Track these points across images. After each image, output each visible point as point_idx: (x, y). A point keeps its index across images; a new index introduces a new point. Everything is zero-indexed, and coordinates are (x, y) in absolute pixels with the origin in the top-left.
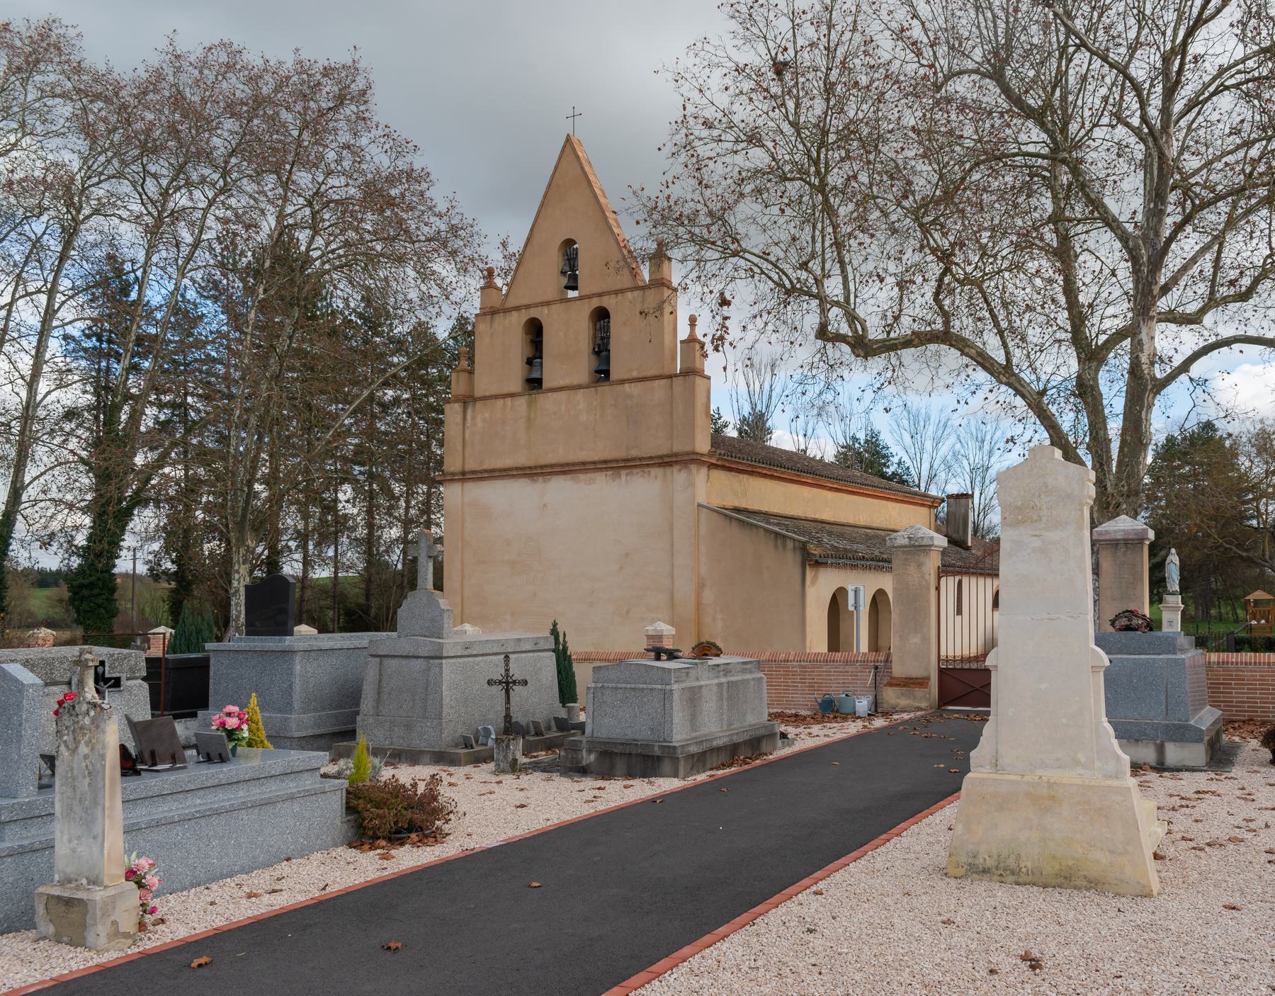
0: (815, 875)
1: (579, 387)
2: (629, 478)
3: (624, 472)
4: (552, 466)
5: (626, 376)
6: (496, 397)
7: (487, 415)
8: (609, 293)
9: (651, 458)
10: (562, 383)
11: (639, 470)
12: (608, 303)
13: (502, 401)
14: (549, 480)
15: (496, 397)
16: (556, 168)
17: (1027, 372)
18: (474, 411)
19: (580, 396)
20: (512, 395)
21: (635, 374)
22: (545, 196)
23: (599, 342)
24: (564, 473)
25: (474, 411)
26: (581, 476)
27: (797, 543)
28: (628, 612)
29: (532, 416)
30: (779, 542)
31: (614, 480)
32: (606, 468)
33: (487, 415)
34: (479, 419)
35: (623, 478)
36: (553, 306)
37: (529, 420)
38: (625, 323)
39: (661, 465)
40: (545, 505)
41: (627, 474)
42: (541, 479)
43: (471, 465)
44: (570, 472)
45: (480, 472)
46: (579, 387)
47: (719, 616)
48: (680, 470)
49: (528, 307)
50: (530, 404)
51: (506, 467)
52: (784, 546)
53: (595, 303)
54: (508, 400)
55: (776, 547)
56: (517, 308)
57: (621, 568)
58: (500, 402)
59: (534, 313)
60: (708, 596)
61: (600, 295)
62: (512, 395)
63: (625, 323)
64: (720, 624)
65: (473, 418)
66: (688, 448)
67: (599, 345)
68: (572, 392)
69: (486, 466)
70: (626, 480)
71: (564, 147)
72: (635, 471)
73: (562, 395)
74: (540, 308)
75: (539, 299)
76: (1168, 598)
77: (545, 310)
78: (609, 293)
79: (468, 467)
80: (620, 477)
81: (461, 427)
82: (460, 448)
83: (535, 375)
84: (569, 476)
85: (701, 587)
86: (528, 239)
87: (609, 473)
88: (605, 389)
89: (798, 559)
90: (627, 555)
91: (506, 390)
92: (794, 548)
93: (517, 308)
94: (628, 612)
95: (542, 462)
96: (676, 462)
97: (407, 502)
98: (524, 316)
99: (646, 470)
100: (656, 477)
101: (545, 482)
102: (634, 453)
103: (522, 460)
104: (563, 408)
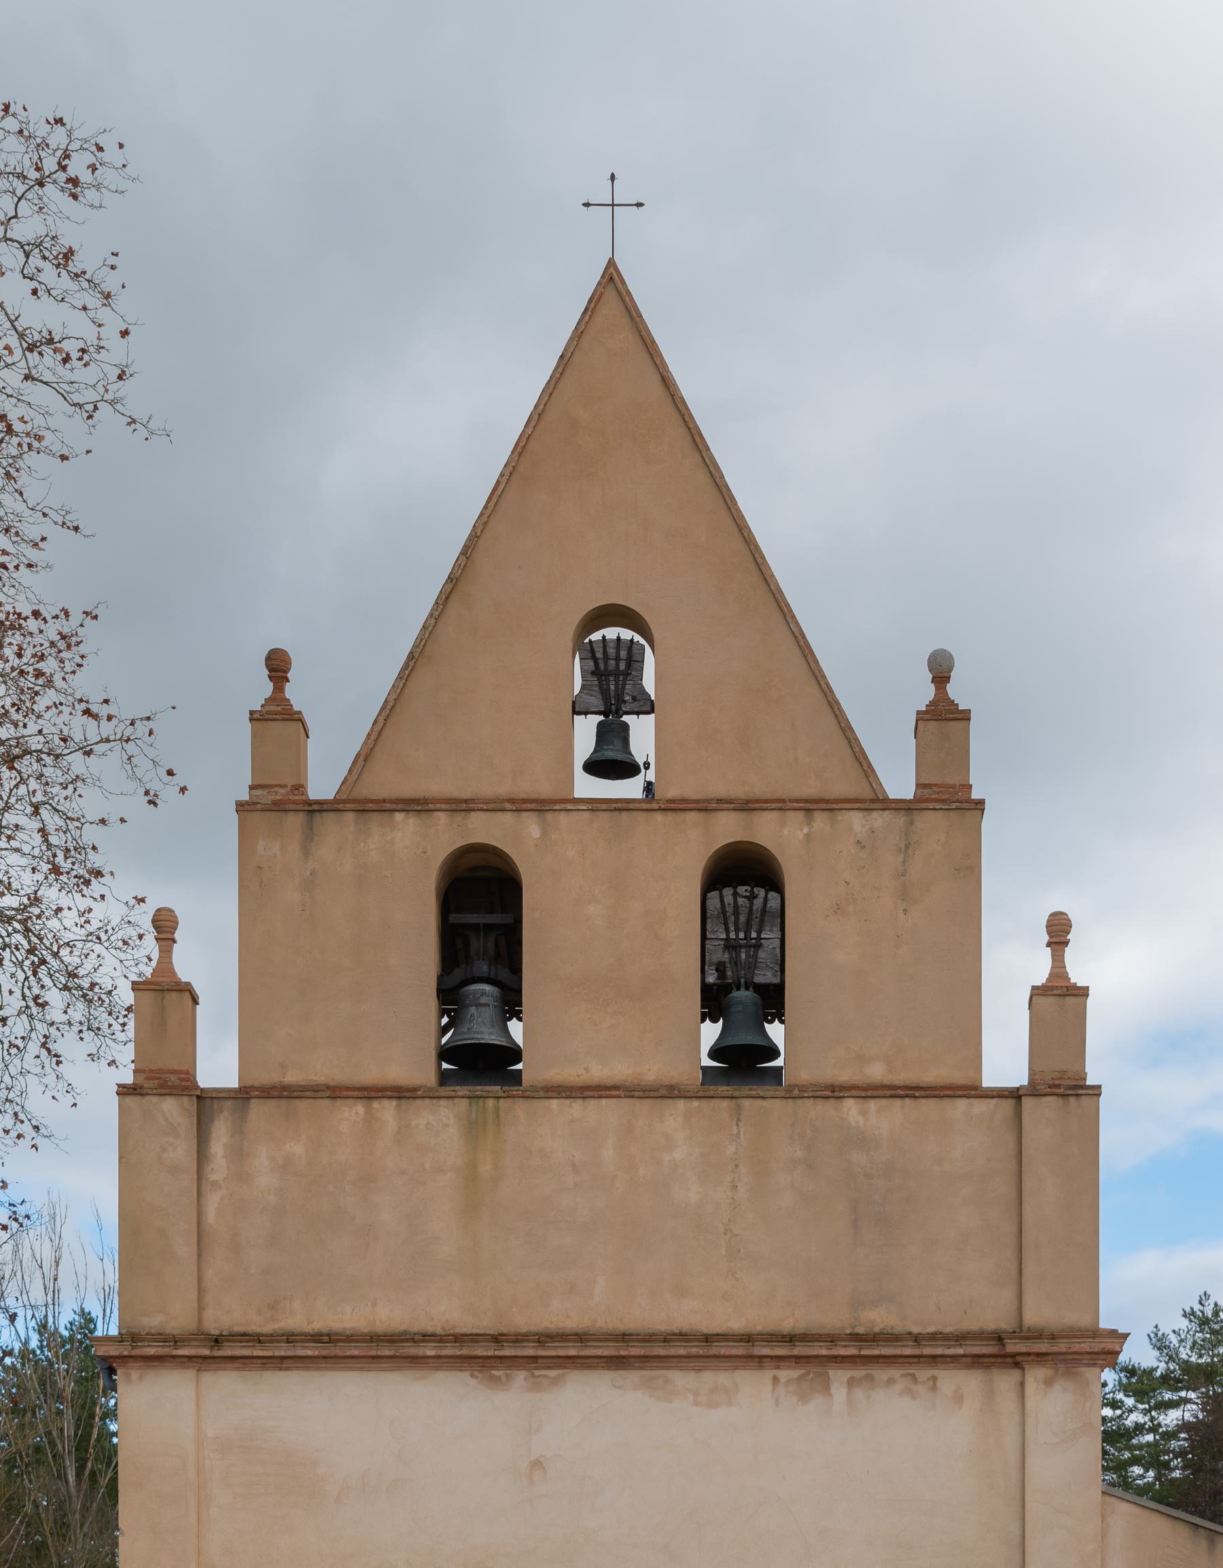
1: (670, 1092)
2: (859, 1393)
3: (839, 1377)
4: (581, 1337)
5: (845, 1076)
6: (336, 1092)
8: (781, 805)
9: (960, 1338)
10: (598, 1072)
11: (895, 1373)
13: (360, 1108)
14: (555, 1381)
15: (336, 1092)
18: (239, 1130)
19: (674, 1116)
20: (401, 1093)
21: (877, 1072)
23: (718, 954)
24: (617, 1363)
26: (681, 1379)
29: (486, 1168)
31: (804, 1398)
33: (297, 1149)
34: (262, 1160)
35: (839, 1392)
36: (563, 818)
37: (470, 1177)
38: (838, 909)
39: (977, 1362)
40: (537, 1464)
41: (851, 1383)
42: (521, 1376)
44: (645, 1361)
46: (670, 1092)
48: (1049, 1383)
49: (461, 806)
50: (473, 1131)
54: (387, 1110)
56: (419, 806)
58: (352, 1113)
61: (747, 806)
62: (401, 1093)
63: (838, 909)
65: (239, 1155)
67: (720, 968)
68: (643, 1107)
70: (850, 1401)
71: (594, 303)
72: (881, 1374)
73: (609, 1112)
74: (508, 818)
75: (502, 789)
76: (1188, 1397)
77: (532, 827)
78: (781, 805)
80: (826, 1388)
87: (785, 1374)
91: (371, 1074)
93: (419, 806)
95: (523, 1321)
96: (1040, 1357)
97: (85, 747)
99: (924, 1374)
100: (958, 1398)
101: (536, 1387)
102: (879, 1318)
104: (608, 1154)
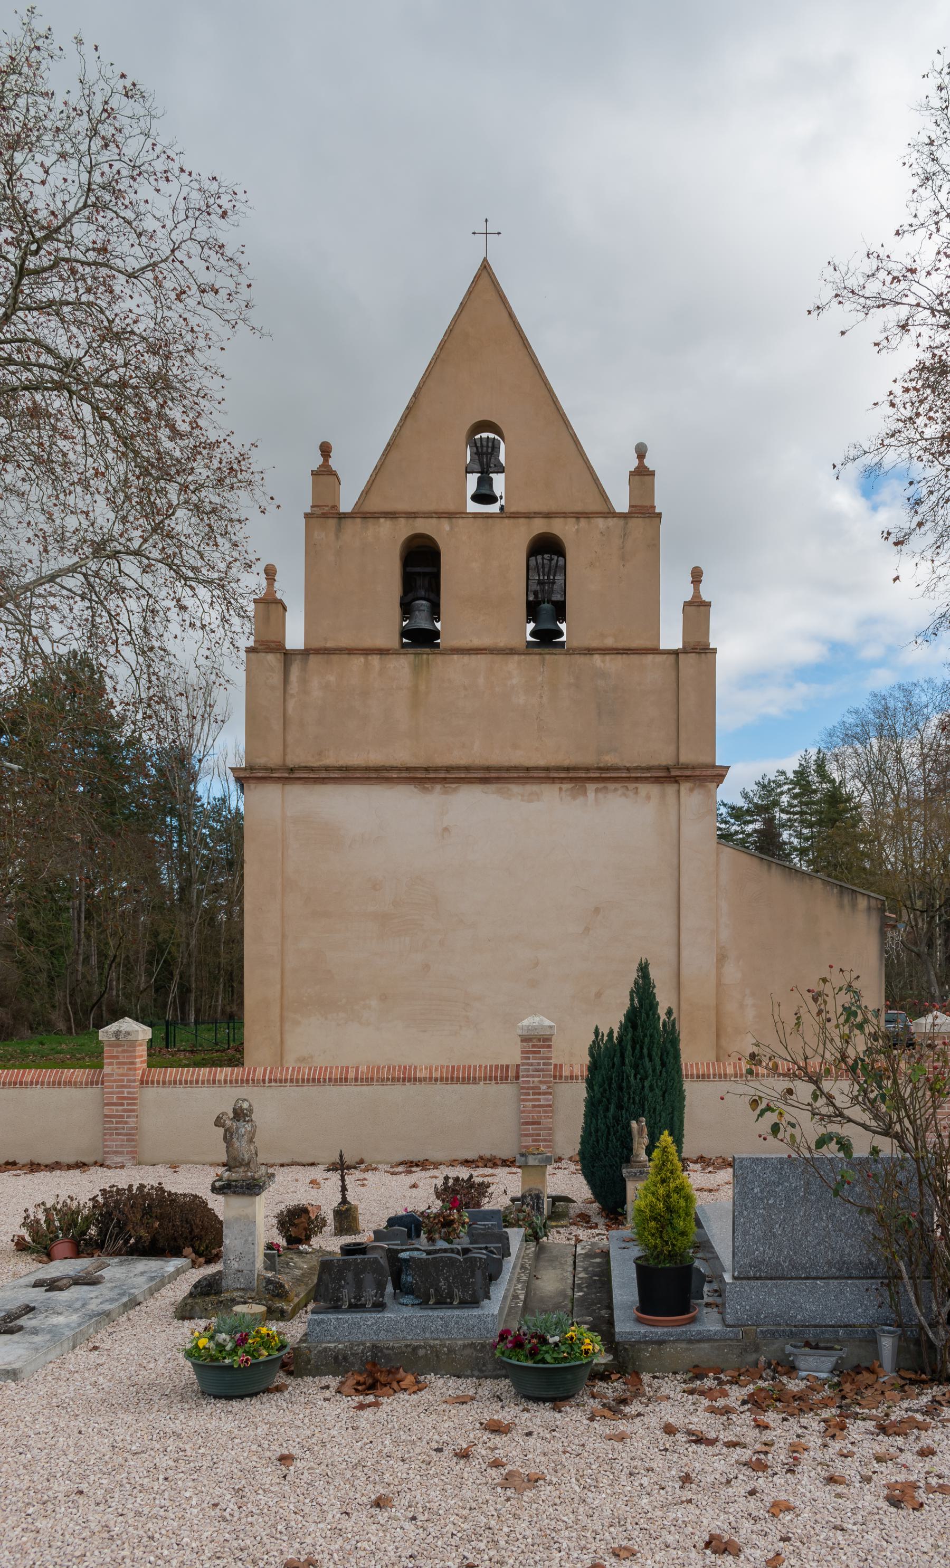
0: (67, 1073)
1: (510, 652)
2: (600, 795)
3: (591, 787)
4: (467, 769)
5: (595, 644)
7: (332, 678)
8: (564, 515)
10: (476, 642)
11: (618, 785)
12: (563, 529)
14: (455, 790)
16: (463, 306)
17: (67, 448)
18: (304, 669)
19: (513, 663)
21: (610, 642)
22: (442, 347)
24: (484, 781)
25: (304, 669)
26: (515, 788)
27: (873, 902)
28: (598, 995)
29: (422, 688)
30: (846, 900)
31: (574, 798)
32: (562, 779)
33: (332, 678)
35: (591, 795)
37: (415, 692)
39: (657, 780)
40: (446, 829)
41: (597, 790)
43: (299, 756)
44: (498, 780)
45: (319, 769)
47: (749, 1001)
48: (692, 790)
49: (412, 515)
50: (416, 670)
51: (371, 764)
52: (854, 905)
53: (539, 527)
54: (375, 660)
55: (841, 906)
56: (392, 515)
57: (587, 929)
58: (359, 661)
59: (423, 527)
60: (732, 973)
61: (548, 516)
64: (750, 1013)
65: (304, 681)
66: (703, 759)
67: (536, 593)
68: (498, 658)
69: (330, 761)
72: (611, 786)
73: (480, 661)
74: (434, 521)
75: (432, 507)
77: (445, 525)
78: (564, 515)
79: (292, 761)
80: (585, 793)
81: (279, 693)
82: (277, 726)
83: (422, 622)
84: (493, 787)
85: (722, 959)
86: (409, 409)
87: (565, 786)
88: (554, 659)
89: (875, 923)
90: (597, 910)
91: (368, 643)
92: (869, 908)
93: (392, 515)
94: (598, 995)
95: (440, 761)
96: (688, 778)
98: (404, 530)
99: (632, 786)
100: (648, 798)
101: (446, 793)
102: (610, 759)
103: (402, 755)
104: (481, 680)
